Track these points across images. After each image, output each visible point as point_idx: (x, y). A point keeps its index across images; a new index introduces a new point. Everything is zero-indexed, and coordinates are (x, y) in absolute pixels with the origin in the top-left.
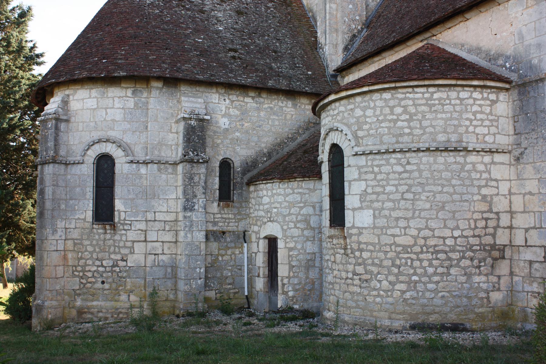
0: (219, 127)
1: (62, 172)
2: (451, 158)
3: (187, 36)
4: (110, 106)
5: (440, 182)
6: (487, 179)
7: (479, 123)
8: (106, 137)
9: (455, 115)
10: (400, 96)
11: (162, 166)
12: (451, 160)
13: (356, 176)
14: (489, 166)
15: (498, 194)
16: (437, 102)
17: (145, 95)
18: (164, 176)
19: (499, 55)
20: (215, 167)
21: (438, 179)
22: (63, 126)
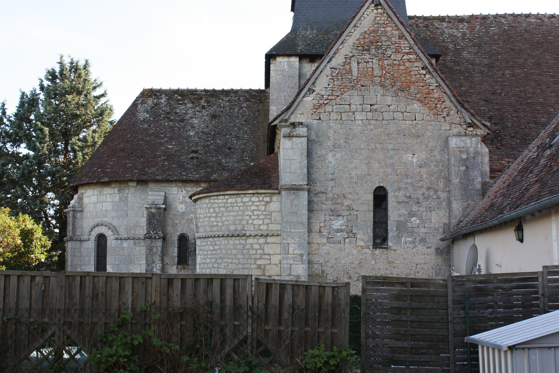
0: (178, 211)
1: (78, 246)
2: (237, 241)
3: (161, 144)
4: (105, 200)
5: (230, 257)
6: (261, 254)
7: (256, 217)
8: (101, 222)
9: (240, 213)
10: (212, 201)
11: (137, 241)
12: (237, 242)
14: (263, 246)
15: (270, 264)
16: (230, 205)
17: (127, 191)
18: (138, 248)
20: (175, 240)
21: (230, 255)
22: (78, 215)
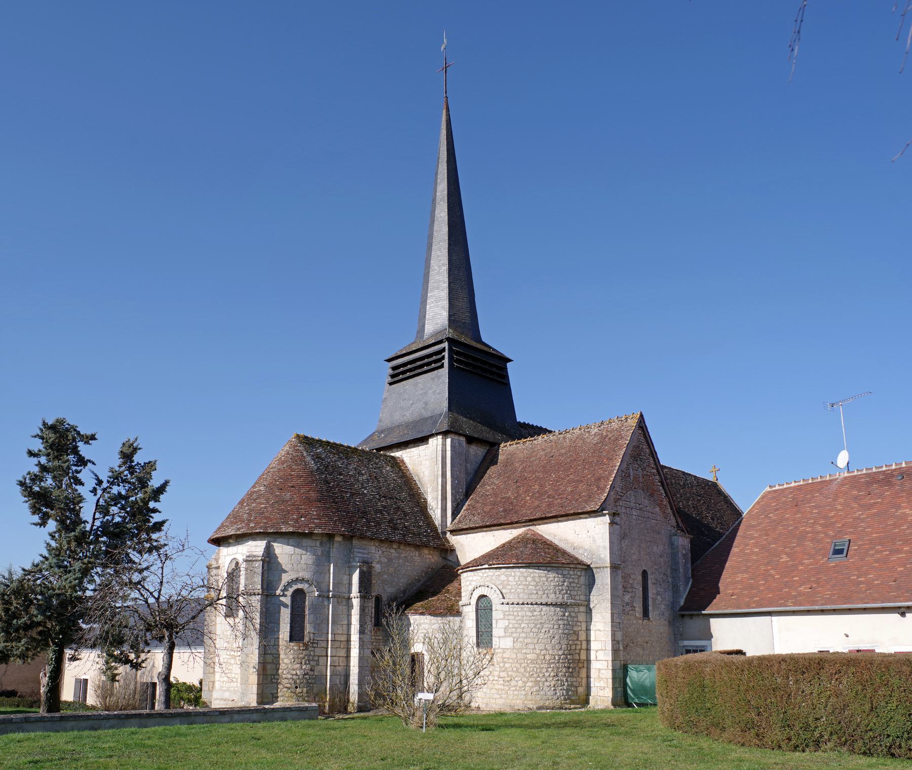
13: (502, 617)
19: (581, 548)
